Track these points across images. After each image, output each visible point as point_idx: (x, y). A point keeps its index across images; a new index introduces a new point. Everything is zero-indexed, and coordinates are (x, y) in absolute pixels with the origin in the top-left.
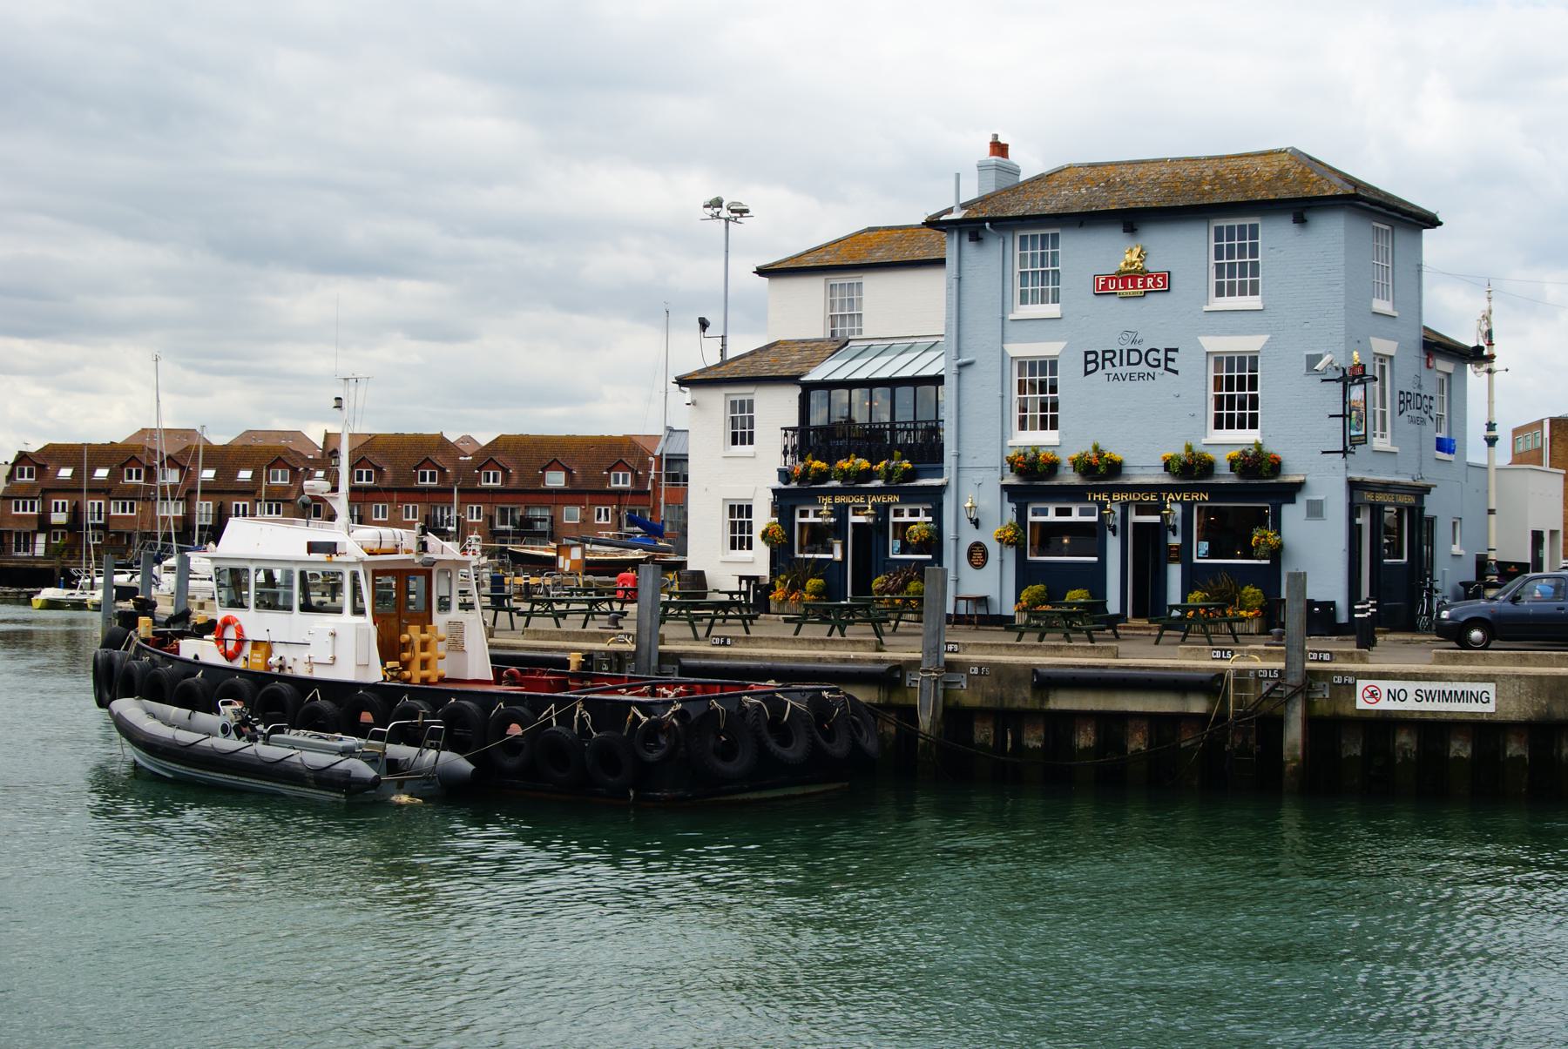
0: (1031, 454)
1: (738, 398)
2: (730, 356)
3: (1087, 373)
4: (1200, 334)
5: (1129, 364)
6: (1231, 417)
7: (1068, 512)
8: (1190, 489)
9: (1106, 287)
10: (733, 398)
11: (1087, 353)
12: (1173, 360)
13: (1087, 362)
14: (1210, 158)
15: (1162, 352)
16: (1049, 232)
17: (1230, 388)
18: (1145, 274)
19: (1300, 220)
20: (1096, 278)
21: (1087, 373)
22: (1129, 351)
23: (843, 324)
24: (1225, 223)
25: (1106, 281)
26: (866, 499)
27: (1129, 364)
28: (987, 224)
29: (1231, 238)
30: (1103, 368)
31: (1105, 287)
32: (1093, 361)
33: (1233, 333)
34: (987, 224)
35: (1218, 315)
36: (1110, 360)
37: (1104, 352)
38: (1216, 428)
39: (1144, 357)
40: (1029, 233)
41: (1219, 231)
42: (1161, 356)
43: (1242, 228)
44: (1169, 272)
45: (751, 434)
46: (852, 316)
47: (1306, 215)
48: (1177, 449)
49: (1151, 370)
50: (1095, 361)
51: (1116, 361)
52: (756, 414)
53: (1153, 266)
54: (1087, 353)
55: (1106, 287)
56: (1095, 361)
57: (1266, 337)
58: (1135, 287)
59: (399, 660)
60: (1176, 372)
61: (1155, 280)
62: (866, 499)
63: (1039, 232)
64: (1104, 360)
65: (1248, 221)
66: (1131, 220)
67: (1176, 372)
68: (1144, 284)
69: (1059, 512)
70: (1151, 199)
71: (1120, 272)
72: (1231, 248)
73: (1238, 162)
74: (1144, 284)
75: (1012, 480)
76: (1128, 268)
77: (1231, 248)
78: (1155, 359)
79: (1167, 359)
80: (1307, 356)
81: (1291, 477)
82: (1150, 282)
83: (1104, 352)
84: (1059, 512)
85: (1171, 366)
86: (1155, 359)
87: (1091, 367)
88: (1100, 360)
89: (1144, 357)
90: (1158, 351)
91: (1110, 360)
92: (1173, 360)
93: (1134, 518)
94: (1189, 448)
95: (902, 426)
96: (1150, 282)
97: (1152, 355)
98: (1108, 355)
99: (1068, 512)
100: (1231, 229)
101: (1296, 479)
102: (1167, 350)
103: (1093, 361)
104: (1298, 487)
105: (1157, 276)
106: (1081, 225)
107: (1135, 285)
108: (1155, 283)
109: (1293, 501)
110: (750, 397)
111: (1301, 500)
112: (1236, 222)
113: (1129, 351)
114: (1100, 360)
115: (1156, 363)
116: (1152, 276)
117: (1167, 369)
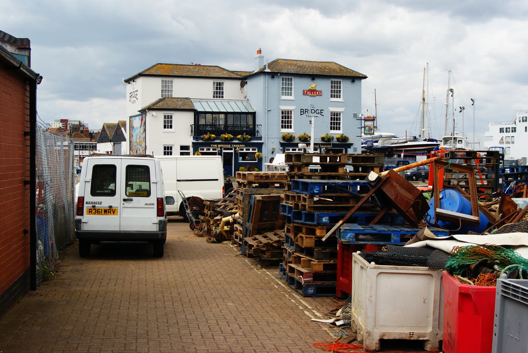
0: (290, 135)
1: (167, 115)
2: (29, 96)
3: (301, 115)
4: (345, 109)
5: (312, 113)
6: (285, 126)
7: (249, 150)
8: (327, 144)
9: (305, 93)
10: (165, 114)
11: (301, 110)
12: (322, 113)
13: (301, 112)
14: (314, 62)
15: (320, 110)
16: (290, 77)
17: (285, 118)
19: (353, 81)
21: (301, 115)
22: (312, 110)
23: (166, 92)
24: (333, 80)
25: (307, 92)
26: (218, 146)
27: (312, 113)
28: (279, 74)
29: (335, 84)
31: (306, 93)
32: (303, 112)
33: (337, 107)
34: (279, 74)
35: (333, 102)
36: (307, 112)
37: (305, 110)
38: (282, 128)
39: (315, 111)
40: (284, 77)
41: (332, 82)
42: (320, 111)
43: (337, 82)
46: (169, 90)
47: (274, 76)
48: (324, 135)
49: (318, 115)
50: (303, 112)
51: (308, 112)
52: (173, 119)
53: (317, 89)
54: (301, 110)
55: (305, 93)
56: (303, 112)
57: (295, 107)
58: (314, 94)
59: (197, 114)
60: (323, 116)
62: (218, 146)
63: (287, 77)
64: (305, 111)
65: (339, 80)
66: (313, 77)
67: (323, 116)
68: (316, 93)
69: (293, 150)
70: (316, 72)
72: (335, 86)
73: (325, 64)
74: (316, 93)
75: (282, 142)
76: (312, 89)
77: (335, 86)
79: (321, 112)
80: (354, 114)
81: (350, 142)
82: (317, 93)
83: (305, 110)
84: (293, 150)
85: (322, 114)
87: (302, 113)
88: (304, 112)
89: (315, 111)
91: (307, 112)
92: (322, 113)
93: (224, 151)
94: (327, 134)
95: (236, 126)
96: (317, 93)
97: (317, 111)
98: (307, 110)
99: (249, 150)
100: (335, 81)
101: (352, 143)
102: (321, 110)
103: (303, 112)
104: (352, 144)
106: (301, 77)
107: (314, 93)
108: (319, 93)
109: (350, 148)
110: (171, 115)
111: (352, 147)
112: (336, 80)
113: (312, 110)
114: (304, 112)
117: (321, 115)
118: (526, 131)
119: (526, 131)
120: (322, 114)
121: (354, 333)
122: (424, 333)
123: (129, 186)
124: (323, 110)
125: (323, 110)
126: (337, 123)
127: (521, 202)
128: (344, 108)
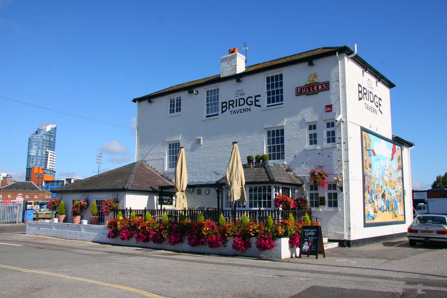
12: (258, 101)
18: (318, 84)
20: (297, 89)
21: (360, 99)
25: (301, 89)
30: (229, 109)
31: (301, 92)
37: (229, 101)
39: (246, 101)
42: (253, 100)
44: (328, 82)
45: (180, 108)
51: (234, 105)
56: (226, 106)
60: (259, 106)
61: (322, 86)
64: (229, 105)
71: (307, 85)
74: (318, 88)
78: (250, 102)
79: (256, 101)
82: (320, 87)
85: (257, 103)
86: (250, 102)
87: (224, 109)
88: (228, 106)
90: (252, 97)
92: (258, 101)
98: (231, 103)
102: (256, 97)
105: (323, 84)
108: (322, 87)
113: (239, 99)
114: (228, 106)
115: (251, 103)
116: (321, 85)
117: (256, 105)
118: (319, 154)
119: (319, 154)
120: (257, 103)
121: (400, 215)
122: (395, 141)
123: (120, 220)
124: (259, 96)
125: (259, 96)
126: (278, 146)
127: (446, 178)
128: (391, 139)
